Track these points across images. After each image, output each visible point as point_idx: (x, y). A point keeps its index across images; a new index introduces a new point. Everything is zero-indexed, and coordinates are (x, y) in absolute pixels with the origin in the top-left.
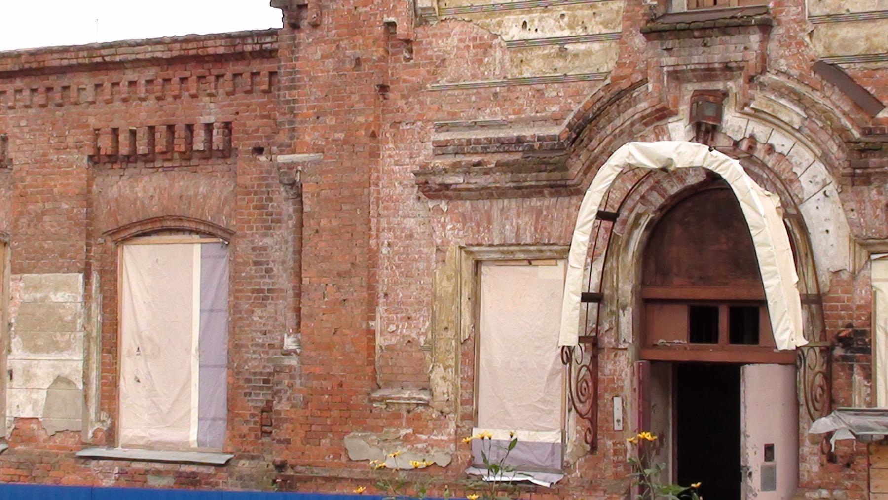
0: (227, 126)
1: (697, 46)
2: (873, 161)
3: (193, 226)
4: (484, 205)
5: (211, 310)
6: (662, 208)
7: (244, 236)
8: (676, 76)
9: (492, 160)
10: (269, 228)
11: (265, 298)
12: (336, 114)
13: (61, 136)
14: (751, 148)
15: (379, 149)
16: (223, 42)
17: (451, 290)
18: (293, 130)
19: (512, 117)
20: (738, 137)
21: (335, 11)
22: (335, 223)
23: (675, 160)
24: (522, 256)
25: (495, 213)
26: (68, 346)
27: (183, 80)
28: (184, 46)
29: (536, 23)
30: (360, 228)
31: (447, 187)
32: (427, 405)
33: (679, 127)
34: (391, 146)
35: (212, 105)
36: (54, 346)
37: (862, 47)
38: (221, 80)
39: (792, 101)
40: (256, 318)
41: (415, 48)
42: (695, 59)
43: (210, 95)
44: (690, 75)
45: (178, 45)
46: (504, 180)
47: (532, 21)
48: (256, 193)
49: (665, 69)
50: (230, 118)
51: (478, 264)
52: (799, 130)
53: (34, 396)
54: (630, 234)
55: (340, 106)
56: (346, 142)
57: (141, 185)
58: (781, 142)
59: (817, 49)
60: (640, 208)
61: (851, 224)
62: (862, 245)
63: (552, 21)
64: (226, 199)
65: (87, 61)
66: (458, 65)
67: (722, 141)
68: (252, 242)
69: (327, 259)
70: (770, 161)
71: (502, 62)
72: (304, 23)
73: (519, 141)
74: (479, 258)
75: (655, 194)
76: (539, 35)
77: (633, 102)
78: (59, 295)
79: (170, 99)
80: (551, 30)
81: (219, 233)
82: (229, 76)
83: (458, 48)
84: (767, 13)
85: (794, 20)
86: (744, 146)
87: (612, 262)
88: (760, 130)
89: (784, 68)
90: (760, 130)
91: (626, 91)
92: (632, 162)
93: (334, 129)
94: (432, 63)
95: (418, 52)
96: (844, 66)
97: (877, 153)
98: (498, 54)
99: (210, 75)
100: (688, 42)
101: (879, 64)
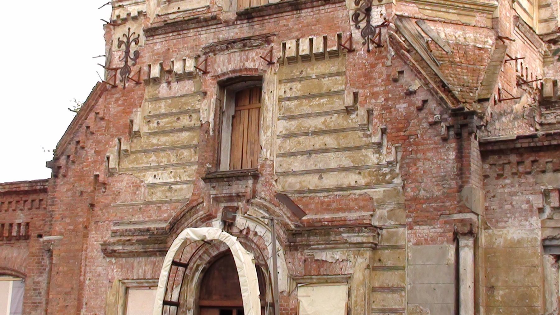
0: (27, 224)
1: (226, 185)
2: (298, 239)
3: (9, 272)
4: (131, 260)
5: (15, 313)
6: (209, 262)
7: (30, 277)
8: (217, 199)
9: (135, 238)
10: (41, 273)
11: (37, 306)
12: (71, 217)
14: (248, 233)
15: (88, 234)
16: (27, 185)
17: (114, 301)
18: (51, 224)
19: (147, 219)
20: (242, 229)
21: (74, 169)
22: (66, 269)
23: (207, 236)
24: (146, 285)
25: (136, 264)
27: (10, 203)
28: (11, 186)
29: (160, 175)
30: (77, 271)
31: (114, 251)
33: (217, 224)
34: (94, 232)
37: (297, 187)
38: (27, 203)
39: (264, 211)
41: (107, 187)
42: (225, 192)
43: (21, 210)
44: (222, 199)
45: (8, 186)
46: (138, 248)
47: (158, 174)
48: (37, 256)
49: (212, 196)
50: (29, 221)
51: (127, 289)
52: (267, 225)
54: (194, 274)
55: (72, 213)
56: (73, 230)
58: (260, 230)
59: (278, 188)
60: (199, 262)
61: (289, 269)
62: (293, 279)
63: (167, 175)
64: (25, 259)
66: (125, 195)
67: (235, 230)
68: (33, 279)
69: (60, 286)
70: (255, 239)
71: (144, 194)
72: (60, 175)
73: (148, 230)
74: (128, 285)
75: (206, 255)
76: (161, 181)
77: (197, 212)
79: (4, 212)
80: (166, 179)
81: (21, 275)
82: (30, 201)
83: (126, 187)
84: (257, 171)
85: (269, 174)
86: (244, 233)
87: (185, 287)
88: (251, 225)
89: (263, 196)
90: (251, 225)
91: (196, 206)
92: (188, 237)
93: (69, 224)
94: (114, 194)
95: (109, 189)
96: (290, 195)
97: (300, 236)
98: (143, 190)
99: (22, 200)
100: (222, 184)
101: (305, 195)
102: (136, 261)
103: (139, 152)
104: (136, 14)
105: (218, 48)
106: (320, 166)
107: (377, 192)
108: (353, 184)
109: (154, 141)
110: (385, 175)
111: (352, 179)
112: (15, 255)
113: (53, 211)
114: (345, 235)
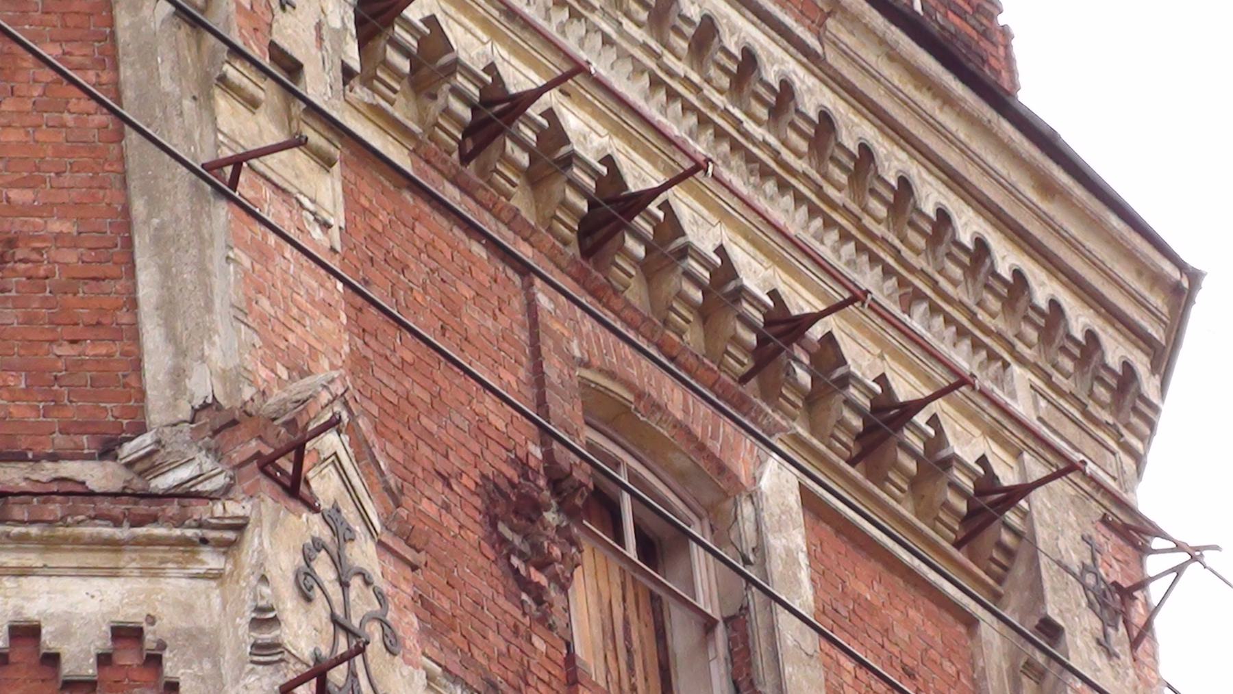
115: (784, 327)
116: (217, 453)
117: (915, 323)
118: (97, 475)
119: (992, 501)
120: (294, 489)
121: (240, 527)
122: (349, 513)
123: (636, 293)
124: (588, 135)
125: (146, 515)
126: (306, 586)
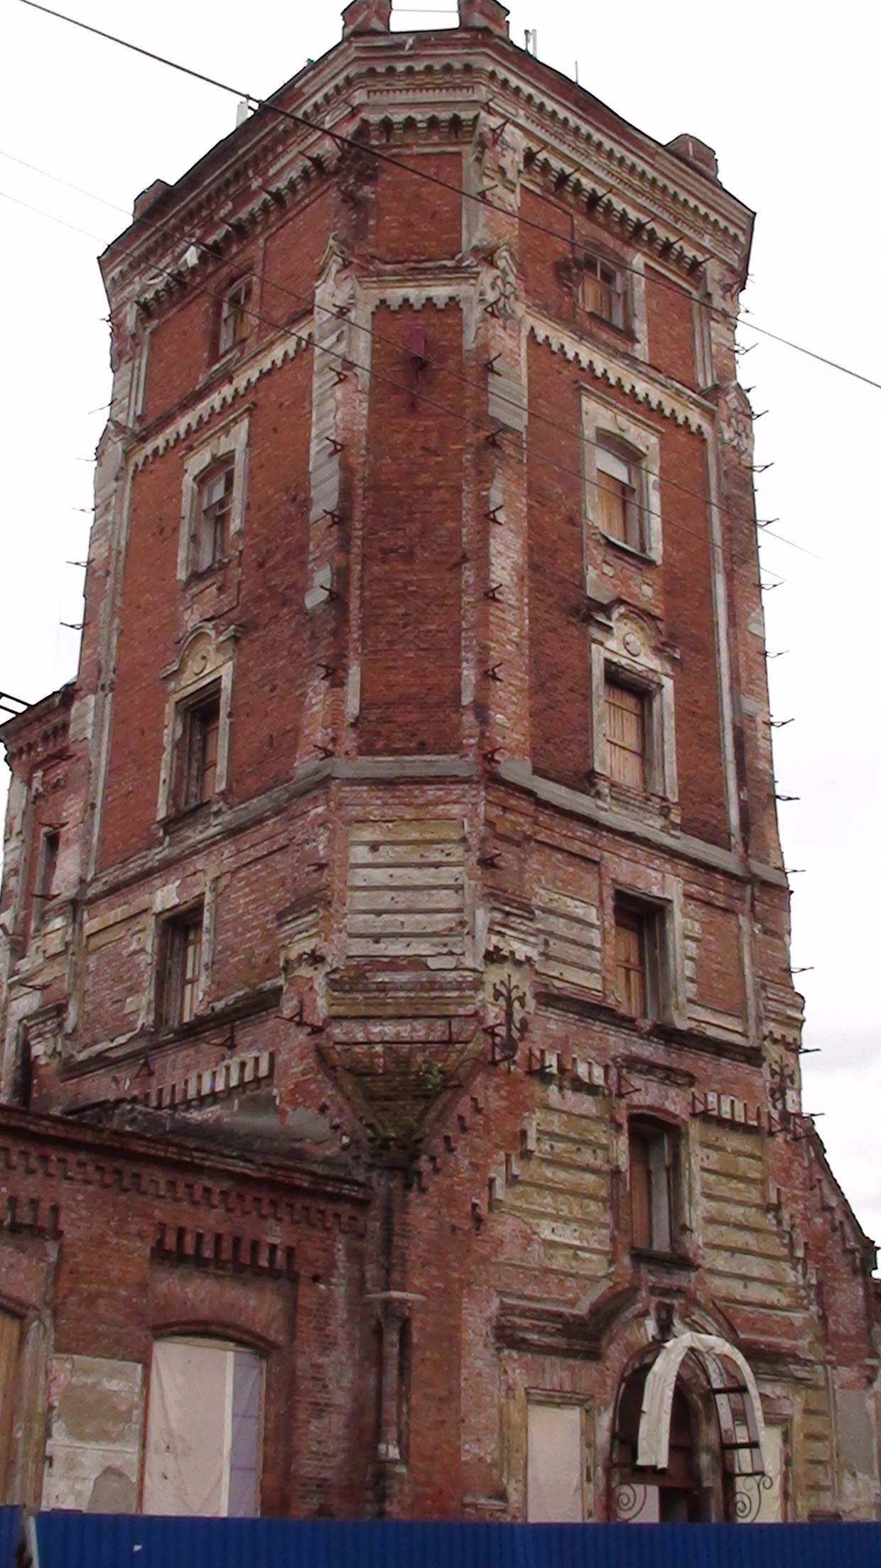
4: (540, 1358)
10: (326, 1349)
13: (123, 1221)
26: (121, 1437)
31: (524, 1340)
32: (504, 1511)
35: (278, 1229)
36: (103, 1435)
37: (723, 1293)
40: (312, 1428)
50: (294, 1244)
53: (78, 1486)
56: (444, 1291)
57: (193, 1286)
65: (175, 1157)
78: (115, 1382)
102: (549, 1361)
103: (529, 1184)
104: (523, 958)
105: (639, 1067)
106: (743, 1271)
107: (798, 1317)
108: (776, 1302)
109: (549, 1172)
110: (803, 1298)
111: (774, 1296)
112: (252, 1303)
113: (407, 1248)
114: (792, 1366)
115: (640, 226)
116: (476, 258)
117: (678, 226)
118: (449, 263)
119: (695, 264)
120: (492, 264)
121: (478, 273)
122: (508, 269)
123: (601, 219)
124: (587, 184)
125: (459, 272)
126: (493, 286)
